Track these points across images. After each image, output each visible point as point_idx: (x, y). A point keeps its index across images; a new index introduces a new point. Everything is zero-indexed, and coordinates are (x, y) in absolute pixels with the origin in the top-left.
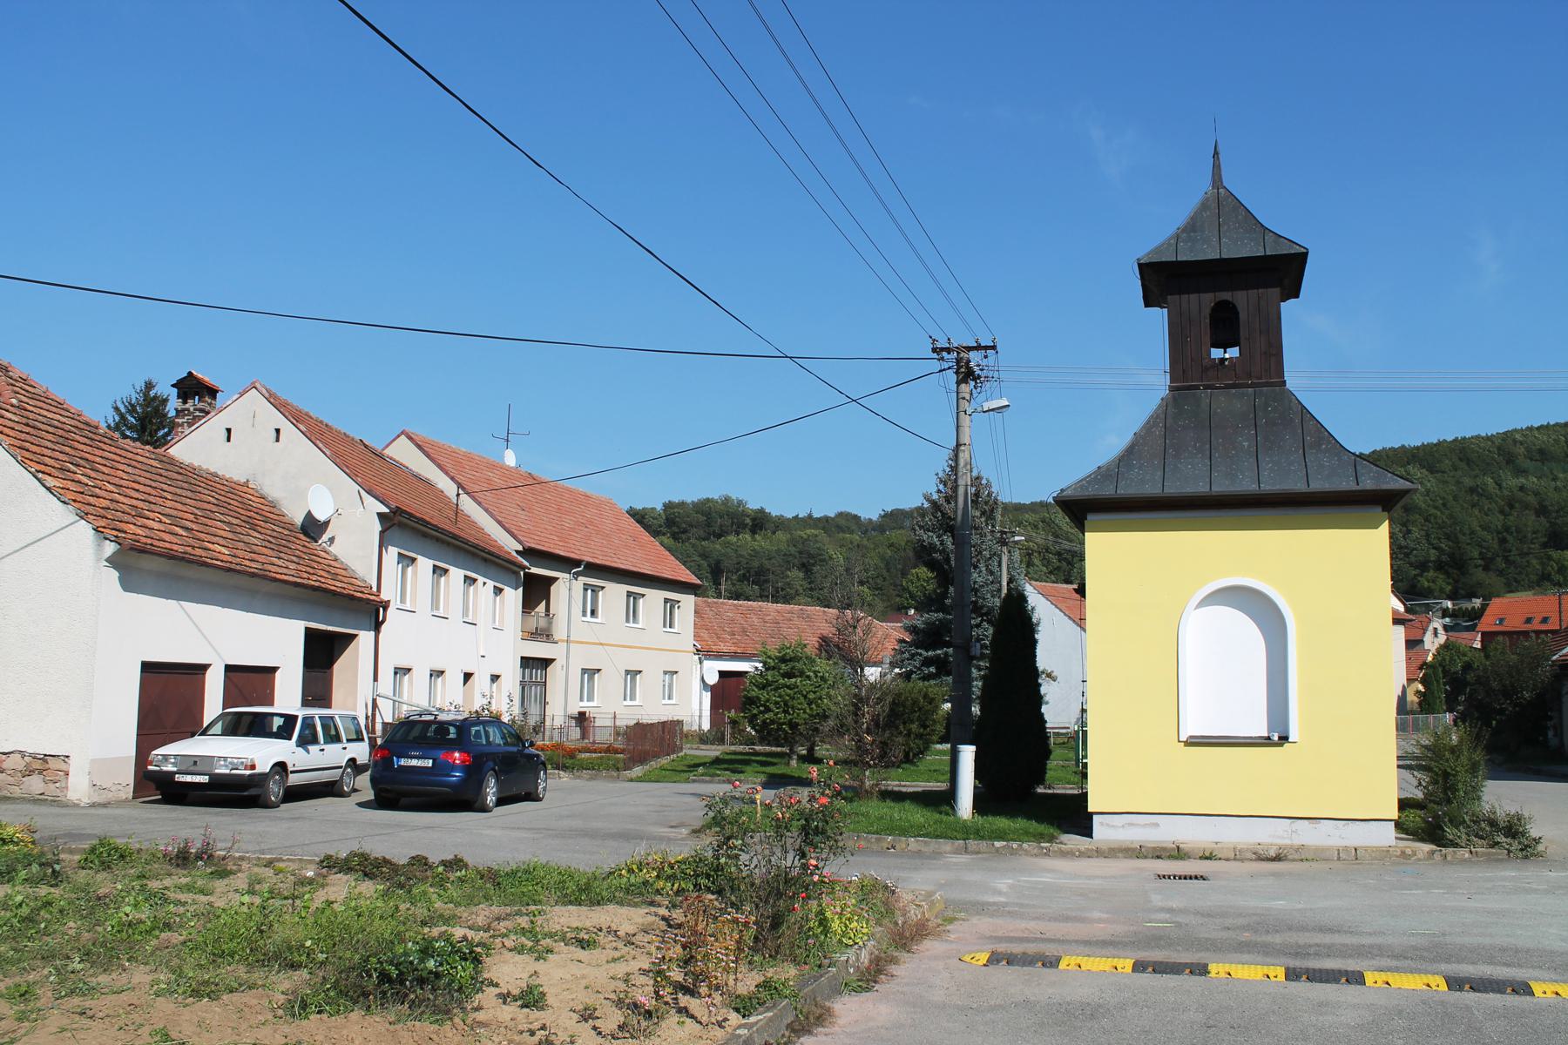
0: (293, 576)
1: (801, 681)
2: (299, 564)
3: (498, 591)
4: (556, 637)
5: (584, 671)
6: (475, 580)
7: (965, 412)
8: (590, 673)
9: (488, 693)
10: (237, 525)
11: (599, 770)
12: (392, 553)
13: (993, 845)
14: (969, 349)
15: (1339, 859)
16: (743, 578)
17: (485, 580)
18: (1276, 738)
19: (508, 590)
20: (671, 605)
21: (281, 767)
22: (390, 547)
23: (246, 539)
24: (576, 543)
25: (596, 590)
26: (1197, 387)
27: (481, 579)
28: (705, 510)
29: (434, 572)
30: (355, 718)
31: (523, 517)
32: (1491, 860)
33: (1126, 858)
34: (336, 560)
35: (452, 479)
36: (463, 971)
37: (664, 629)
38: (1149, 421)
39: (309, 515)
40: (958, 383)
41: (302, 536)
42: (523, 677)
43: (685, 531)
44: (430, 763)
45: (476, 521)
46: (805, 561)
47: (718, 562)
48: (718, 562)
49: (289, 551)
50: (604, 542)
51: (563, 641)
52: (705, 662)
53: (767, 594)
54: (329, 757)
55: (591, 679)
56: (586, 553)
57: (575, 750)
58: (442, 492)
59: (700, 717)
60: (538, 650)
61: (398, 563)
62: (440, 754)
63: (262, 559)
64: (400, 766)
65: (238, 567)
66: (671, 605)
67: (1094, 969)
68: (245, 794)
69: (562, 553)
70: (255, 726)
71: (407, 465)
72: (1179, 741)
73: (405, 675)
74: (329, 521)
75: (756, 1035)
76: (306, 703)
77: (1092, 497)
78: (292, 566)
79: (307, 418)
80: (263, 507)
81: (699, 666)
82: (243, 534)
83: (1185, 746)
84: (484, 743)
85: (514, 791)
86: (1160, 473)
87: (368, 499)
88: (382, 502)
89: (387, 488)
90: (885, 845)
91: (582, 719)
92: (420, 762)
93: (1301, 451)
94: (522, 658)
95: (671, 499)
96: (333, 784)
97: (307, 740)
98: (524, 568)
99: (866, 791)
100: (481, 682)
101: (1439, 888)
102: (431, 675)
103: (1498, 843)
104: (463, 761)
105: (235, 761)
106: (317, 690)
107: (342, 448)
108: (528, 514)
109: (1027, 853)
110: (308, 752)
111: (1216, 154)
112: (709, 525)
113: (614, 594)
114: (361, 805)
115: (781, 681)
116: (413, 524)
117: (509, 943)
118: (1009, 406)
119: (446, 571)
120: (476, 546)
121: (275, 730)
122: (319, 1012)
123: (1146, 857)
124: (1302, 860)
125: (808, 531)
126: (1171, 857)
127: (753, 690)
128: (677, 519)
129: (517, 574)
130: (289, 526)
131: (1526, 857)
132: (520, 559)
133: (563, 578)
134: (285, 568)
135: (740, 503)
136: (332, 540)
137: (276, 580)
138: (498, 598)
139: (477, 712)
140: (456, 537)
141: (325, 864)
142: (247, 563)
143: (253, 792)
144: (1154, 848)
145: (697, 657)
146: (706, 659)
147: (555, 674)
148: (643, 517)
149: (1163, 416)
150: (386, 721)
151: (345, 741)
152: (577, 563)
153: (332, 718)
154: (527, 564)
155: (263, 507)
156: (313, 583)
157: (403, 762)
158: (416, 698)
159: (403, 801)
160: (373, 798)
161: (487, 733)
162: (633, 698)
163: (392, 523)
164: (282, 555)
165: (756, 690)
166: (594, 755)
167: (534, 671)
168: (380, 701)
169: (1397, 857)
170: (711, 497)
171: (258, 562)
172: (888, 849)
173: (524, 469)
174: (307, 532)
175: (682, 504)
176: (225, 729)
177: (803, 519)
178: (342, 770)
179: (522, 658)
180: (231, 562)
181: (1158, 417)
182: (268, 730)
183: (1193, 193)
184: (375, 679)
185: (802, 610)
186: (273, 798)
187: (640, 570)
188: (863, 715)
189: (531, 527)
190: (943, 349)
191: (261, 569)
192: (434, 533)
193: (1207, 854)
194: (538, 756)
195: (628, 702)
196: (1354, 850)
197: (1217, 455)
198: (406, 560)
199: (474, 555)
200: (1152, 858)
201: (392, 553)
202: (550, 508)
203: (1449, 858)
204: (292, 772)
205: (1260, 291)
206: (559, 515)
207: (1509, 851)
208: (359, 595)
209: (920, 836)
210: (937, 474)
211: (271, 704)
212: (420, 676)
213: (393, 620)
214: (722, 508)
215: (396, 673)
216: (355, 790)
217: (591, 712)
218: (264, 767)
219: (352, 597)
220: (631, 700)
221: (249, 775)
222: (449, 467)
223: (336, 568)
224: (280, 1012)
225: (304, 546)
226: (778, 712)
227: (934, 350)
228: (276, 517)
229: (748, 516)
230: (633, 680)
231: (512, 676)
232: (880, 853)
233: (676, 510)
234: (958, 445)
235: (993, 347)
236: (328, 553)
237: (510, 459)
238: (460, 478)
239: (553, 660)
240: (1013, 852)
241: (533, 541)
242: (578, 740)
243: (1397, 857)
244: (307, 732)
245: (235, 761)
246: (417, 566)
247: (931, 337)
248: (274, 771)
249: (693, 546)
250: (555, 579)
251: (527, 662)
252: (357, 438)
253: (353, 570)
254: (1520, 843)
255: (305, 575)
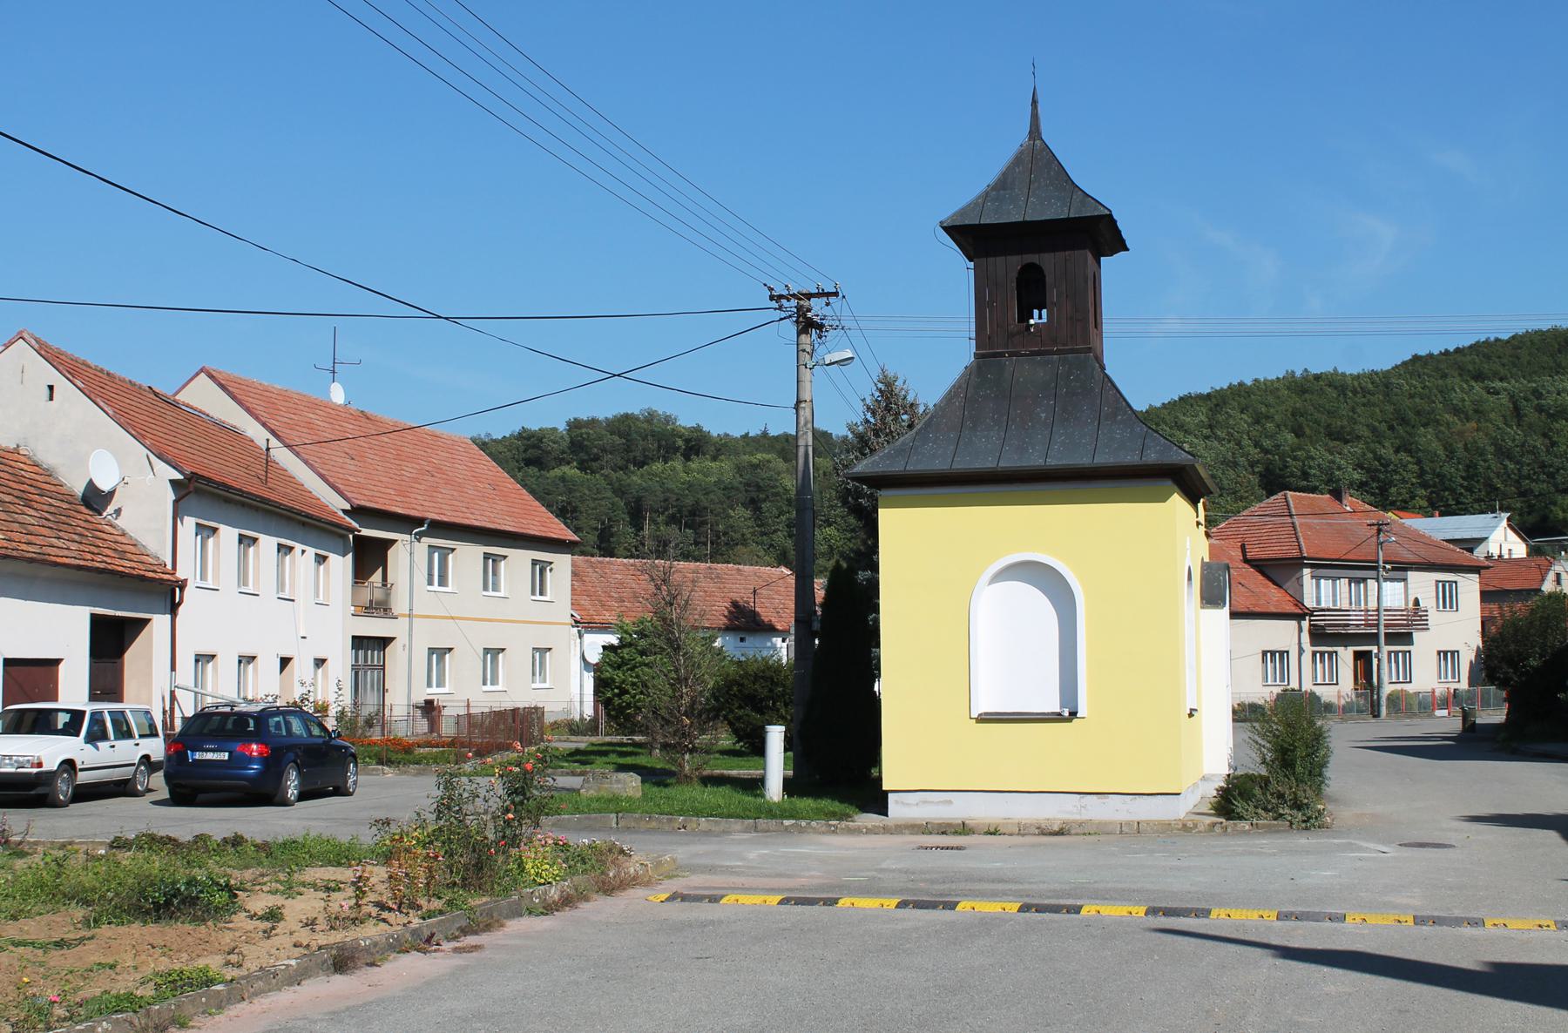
0: (75, 558)
1: (661, 659)
2: (81, 543)
3: (321, 559)
4: (395, 612)
5: (432, 651)
6: (291, 549)
7: (805, 365)
8: (440, 653)
9: (308, 681)
10: (9, 503)
11: (427, 764)
12: (189, 524)
13: (782, 823)
14: (809, 296)
15: (1121, 832)
16: (673, 520)
17: (304, 547)
18: (1066, 714)
19: (334, 559)
20: (541, 568)
21: (69, 764)
22: (186, 517)
23: (20, 518)
24: (419, 497)
25: (445, 553)
26: (1002, 355)
27: (298, 547)
28: (623, 426)
29: (240, 542)
30: (147, 712)
31: (352, 468)
32: (1270, 830)
33: (911, 834)
34: (124, 534)
35: (264, 425)
36: (220, 898)
37: (534, 598)
38: (950, 391)
39: (91, 483)
40: (799, 333)
41: (83, 509)
42: (356, 660)
43: (596, 458)
44: (226, 756)
45: (294, 475)
46: (754, 495)
47: (639, 500)
48: (639, 500)
49: (70, 529)
50: (455, 493)
51: (404, 615)
52: (585, 635)
53: (703, 539)
54: (120, 753)
55: (441, 660)
56: (430, 509)
57: (413, 745)
58: (253, 441)
59: (581, 702)
60: (374, 627)
61: (197, 535)
62: (237, 747)
63: (39, 540)
64: (194, 760)
65: (14, 553)
66: (541, 568)
67: (747, 903)
68: (32, 793)
69: (400, 511)
70: (41, 723)
71: (207, 412)
72: (971, 718)
73: (208, 662)
74: (115, 490)
75: (425, 928)
76: (93, 697)
77: (880, 474)
78: (74, 546)
79: (84, 368)
80: (37, 477)
81: (578, 640)
82: (17, 513)
83: (977, 722)
84: (284, 734)
85: (319, 784)
86: (952, 448)
87: (160, 465)
88: (174, 468)
89: (182, 447)
90: (677, 826)
91: (429, 708)
92: (216, 755)
93: (1097, 422)
94: (354, 637)
95: (576, 416)
96: (125, 782)
97: (97, 735)
98: (352, 530)
99: (686, 776)
100: (302, 667)
101: (1159, 853)
102: (240, 662)
103: (1281, 815)
104: (261, 753)
105: (21, 759)
106: (106, 683)
107: (128, 401)
108: (359, 464)
109: (816, 831)
110: (97, 748)
111: (1034, 102)
112: (628, 450)
113: (468, 556)
114: (155, 803)
115: (639, 659)
116: (212, 489)
117: (265, 888)
118: (852, 358)
119: (255, 540)
120: (291, 510)
121: (60, 726)
122: (109, 923)
123: (931, 833)
124: (1084, 834)
125: (759, 456)
126: (956, 833)
127: (607, 671)
128: (586, 443)
129: (345, 537)
130: (68, 497)
131: (1307, 829)
132: (348, 519)
133: (402, 540)
134: (67, 550)
135: (668, 419)
136: (118, 512)
137: (56, 564)
138: (322, 567)
139: (295, 702)
140: (264, 500)
141: (115, 845)
142: (24, 547)
143: (40, 790)
144: (940, 824)
145: (576, 630)
146: (587, 632)
147: (395, 656)
148: (540, 440)
149: (964, 386)
150: (186, 715)
151: (137, 737)
152: (419, 522)
153: (122, 713)
154: (357, 526)
155: (37, 477)
156: (98, 565)
157: (198, 756)
158: (222, 688)
159: (201, 797)
160: (168, 796)
161: (288, 725)
162: (494, 682)
163: (187, 491)
164: (61, 534)
165: (610, 670)
166: (435, 750)
167: (369, 652)
168: (178, 693)
169: (1179, 830)
170: (630, 412)
171: (35, 544)
172: (679, 829)
173: (354, 406)
174: (89, 503)
175: (593, 422)
176: (7, 728)
177: (755, 439)
178: (134, 768)
179: (354, 637)
180: (6, 548)
181: (960, 387)
182: (53, 728)
183: (1011, 141)
184: (173, 668)
185: (710, 568)
186: (61, 797)
187: (499, 527)
188: (682, 697)
189: (362, 481)
190: (781, 297)
191: (39, 553)
192: (238, 497)
193: (992, 830)
194: (346, 748)
195: (489, 687)
196: (1136, 824)
197: (1013, 427)
198: (206, 532)
199: (289, 519)
200: (938, 833)
201: (189, 524)
202: (388, 455)
203: (1229, 830)
204: (81, 770)
205: (1067, 253)
206: (397, 462)
207: (1291, 823)
208: (151, 575)
209: (712, 816)
210: (863, 400)
211: (55, 699)
212: (226, 665)
213: (191, 600)
214: (645, 425)
215: (197, 661)
216: (150, 790)
217: (440, 700)
218: (51, 765)
219: (143, 578)
220: (492, 684)
221: (37, 773)
222: (260, 411)
223: (125, 546)
224: (80, 926)
225: (87, 521)
226: (635, 695)
227: (772, 298)
228: (53, 488)
229: (680, 437)
230: (495, 660)
231: (341, 660)
232: (674, 831)
233: (584, 430)
234: (799, 402)
235: (836, 294)
236: (114, 528)
237: (338, 395)
238: (273, 423)
239: (392, 639)
240: (802, 831)
241: (363, 497)
242: (425, 734)
243: (1179, 830)
244: (96, 728)
245: (21, 759)
246: (219, 537)
247: (765, 285)
248: (61, 768)
249: (606, 477)
250: (393, 542)
251: (359, 642)
252: (145, 384)
253: (144, 546)
254: (1303, 815)
255: (89, 556)
